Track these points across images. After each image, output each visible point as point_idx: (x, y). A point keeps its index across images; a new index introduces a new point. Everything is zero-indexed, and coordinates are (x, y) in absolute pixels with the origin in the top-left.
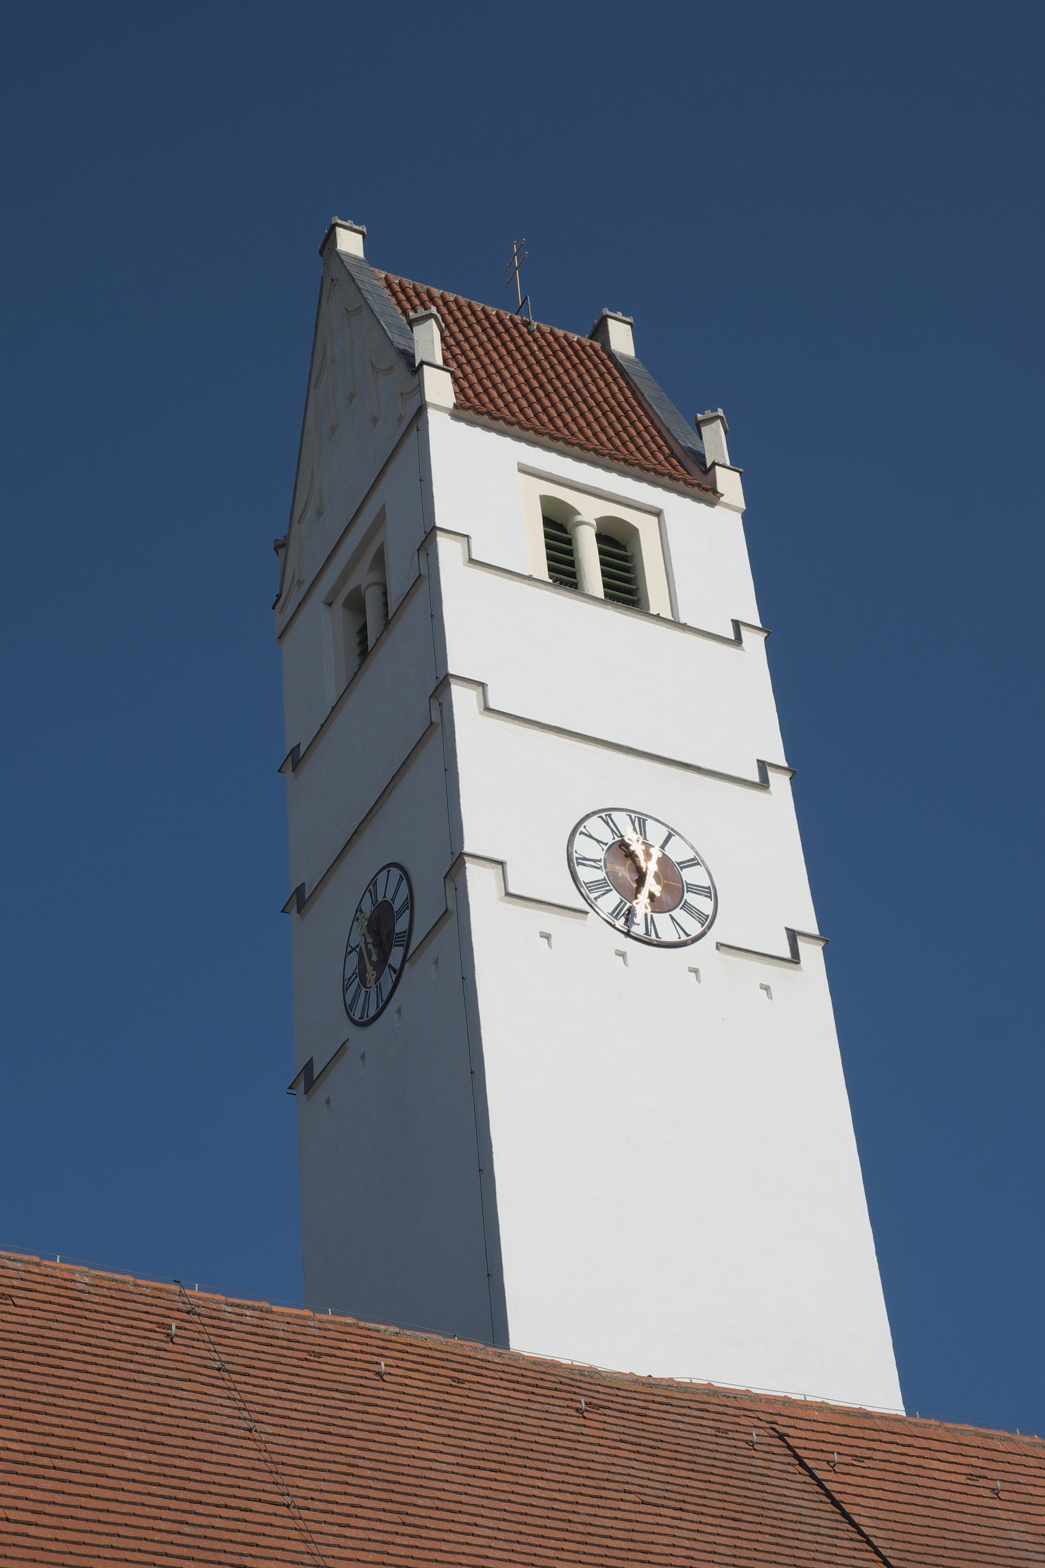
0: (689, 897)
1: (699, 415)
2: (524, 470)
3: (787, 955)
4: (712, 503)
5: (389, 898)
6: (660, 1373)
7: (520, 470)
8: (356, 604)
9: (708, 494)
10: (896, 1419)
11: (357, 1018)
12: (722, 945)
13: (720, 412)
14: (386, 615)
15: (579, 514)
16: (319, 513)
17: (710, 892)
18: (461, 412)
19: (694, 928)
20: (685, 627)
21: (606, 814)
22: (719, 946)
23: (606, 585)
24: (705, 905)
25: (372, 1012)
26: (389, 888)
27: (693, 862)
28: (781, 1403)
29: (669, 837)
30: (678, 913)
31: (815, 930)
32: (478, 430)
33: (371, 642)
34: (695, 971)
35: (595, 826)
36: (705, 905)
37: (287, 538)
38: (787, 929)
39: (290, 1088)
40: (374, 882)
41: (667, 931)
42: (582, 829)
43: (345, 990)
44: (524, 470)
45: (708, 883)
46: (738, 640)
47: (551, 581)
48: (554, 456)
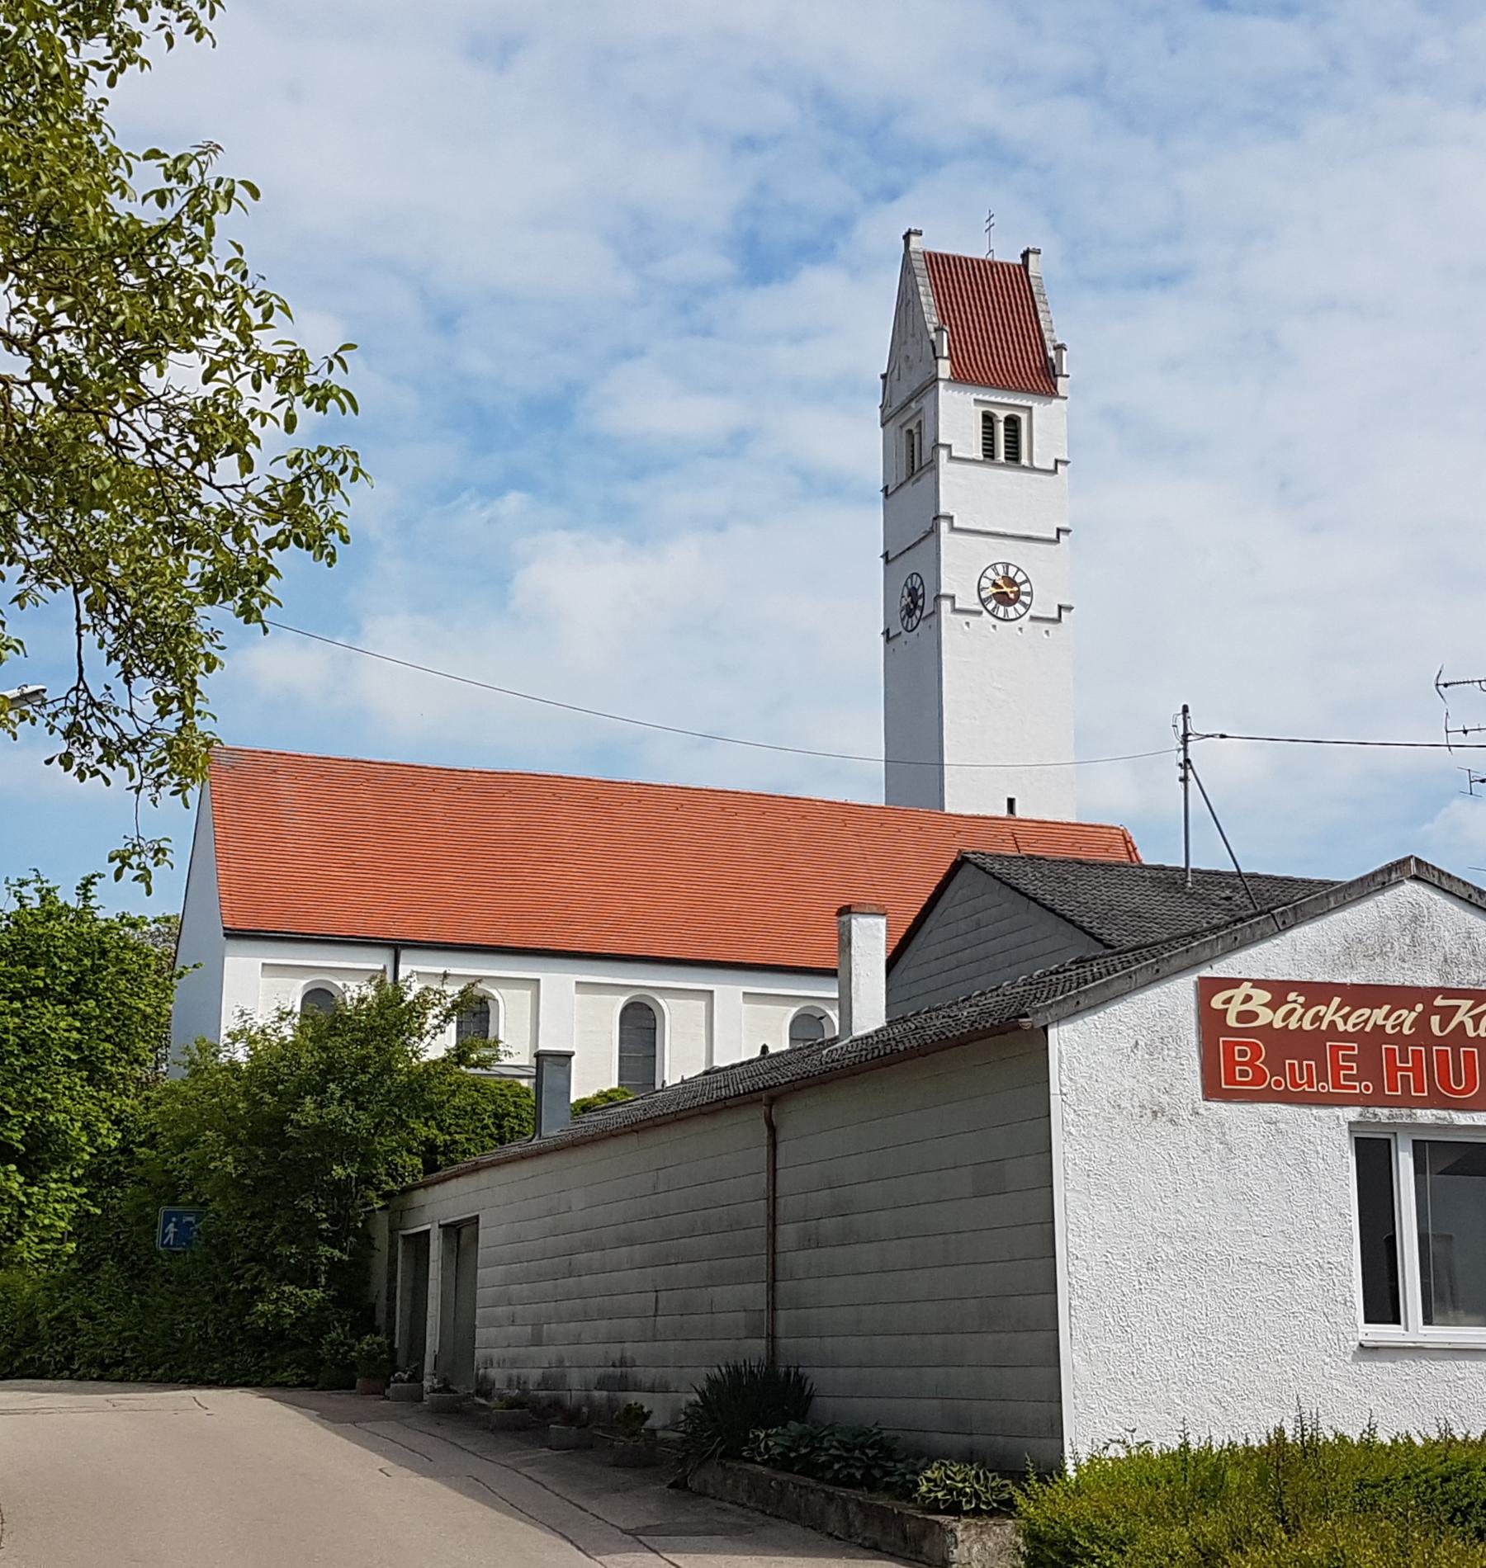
30: (1017, 606)
41: (1012, 614)
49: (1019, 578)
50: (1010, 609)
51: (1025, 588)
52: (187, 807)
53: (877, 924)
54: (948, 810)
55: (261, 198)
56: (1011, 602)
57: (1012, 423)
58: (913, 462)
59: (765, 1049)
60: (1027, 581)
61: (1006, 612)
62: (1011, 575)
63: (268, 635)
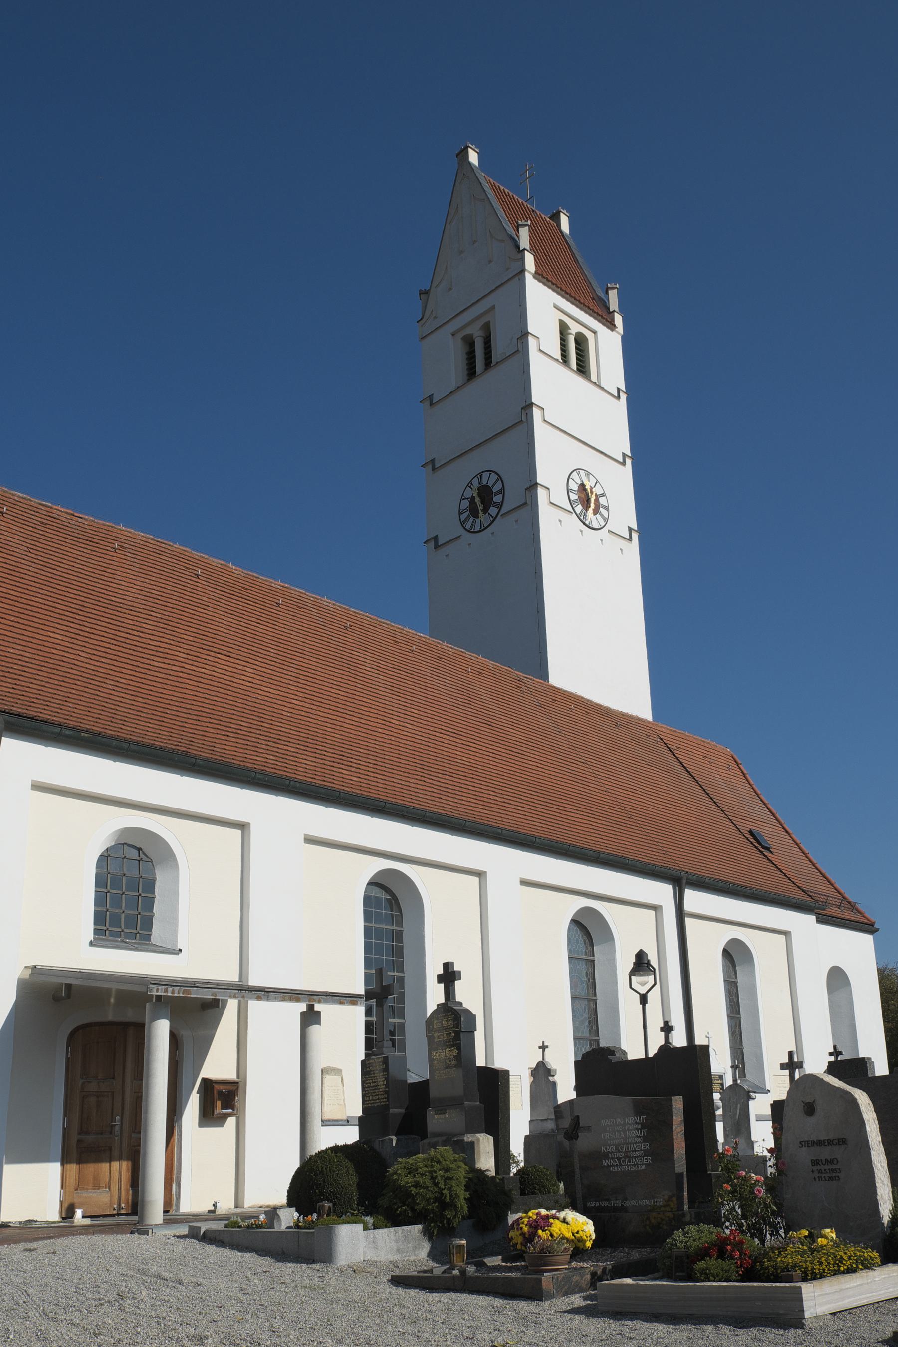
1: (609, 285)
2: (556, 307)
3: (628, 537)
4: (612, 330)
5: (490, 484)
6: (625, 710)
7: (555, 307)
9: (611, 326)
10: (649, 722)
13: (618, 286)
15: (570, 329)
17: (606, 508)
18: (537, 276)
20: (602, 389)
22: (609, 531)
23: (577, 364)
31: (636, 528)
32: (541, 284)
34: (601, 540)
37: (429, 290)
38: (629, 527)
39: (424, 543)
42: (492, 519)
44: (556, 307)
45: (607, 505)
47: (562, 361)
48: (564, 300)
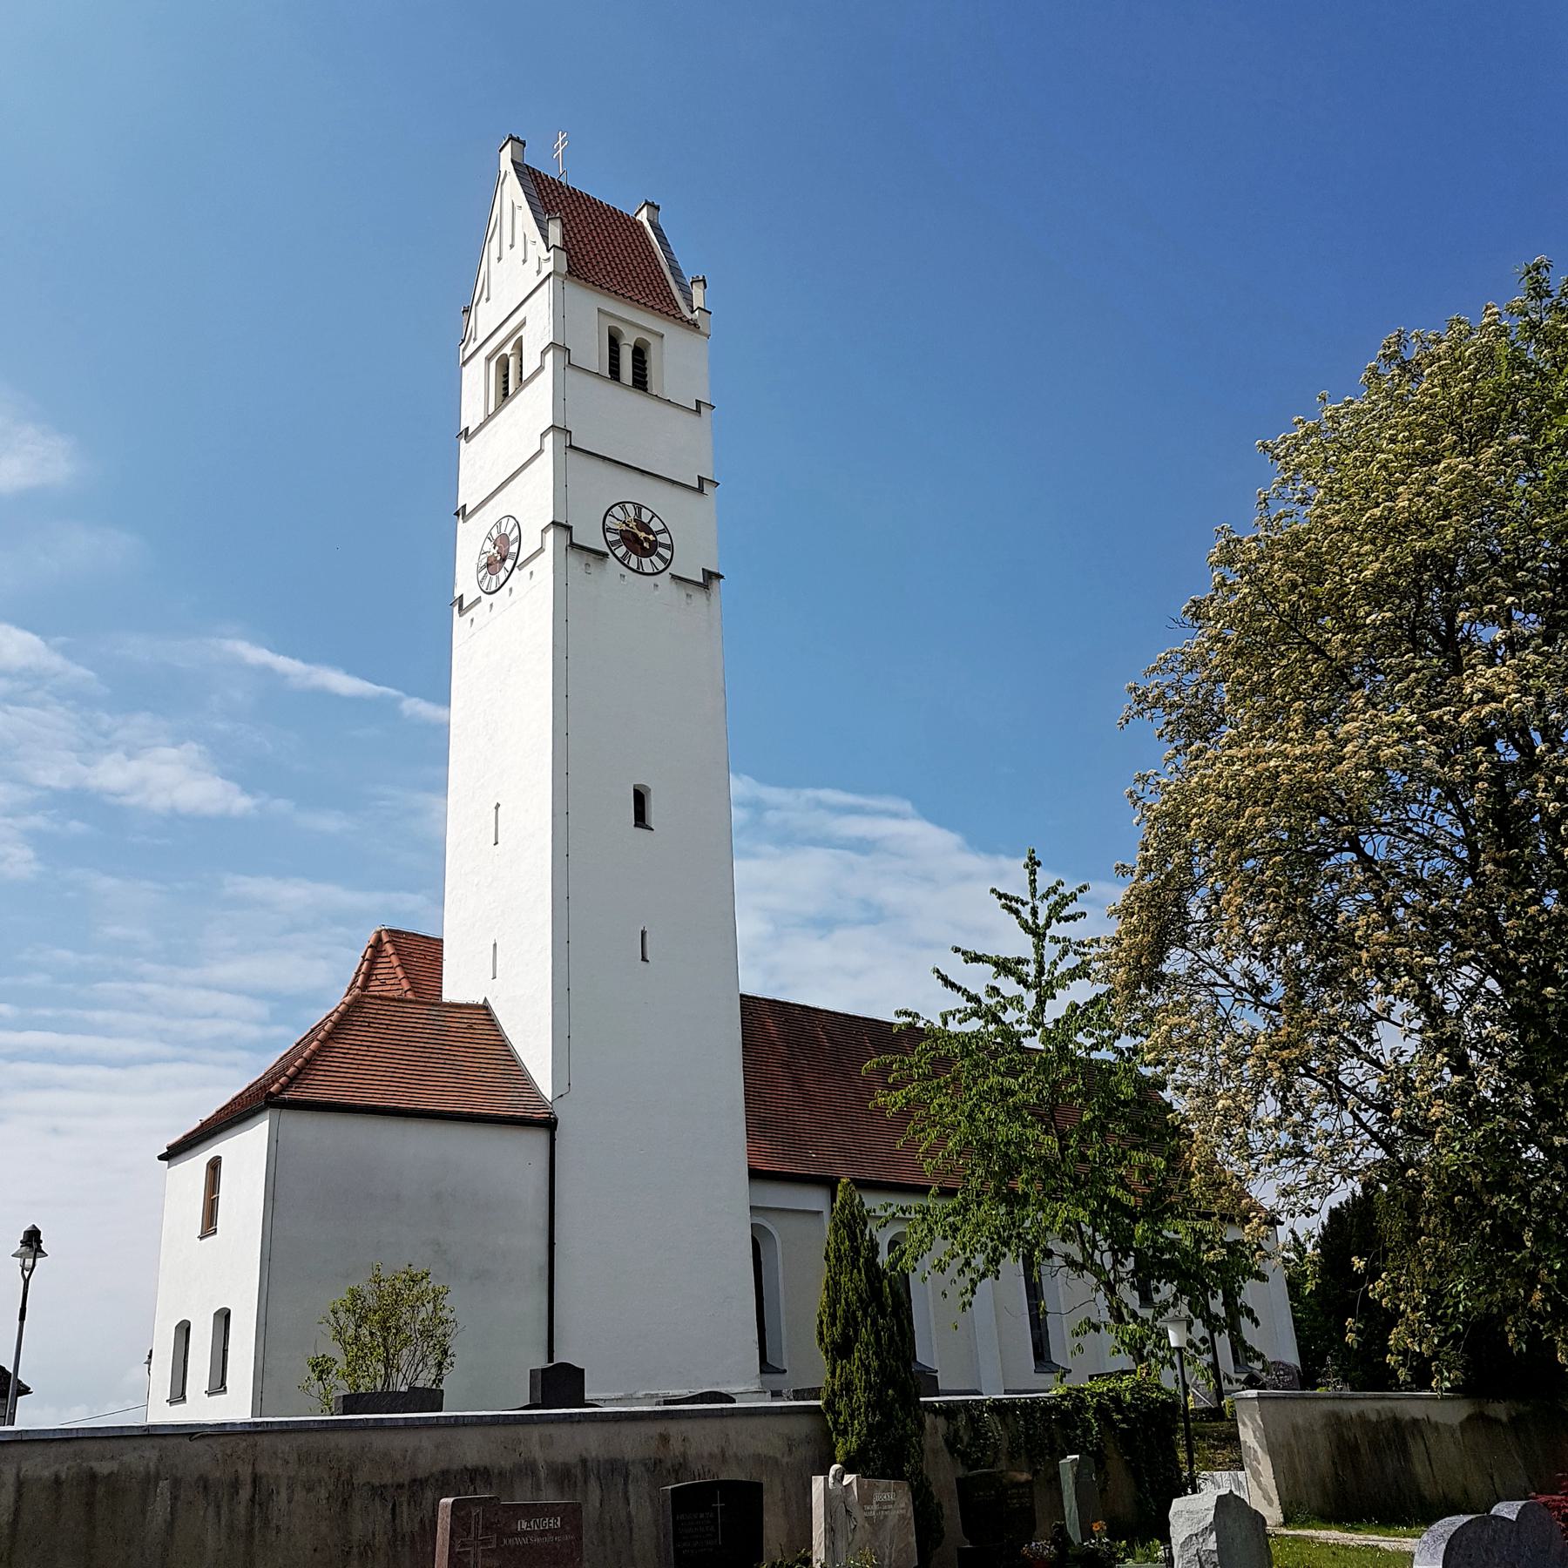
0: (659, 549)
5: (507, 533)
8: (504, 364)
11: (484, 588)
12: (188, 1330)
14: (521, 379)
16: (488, 300)
17: (670, 547)
19: (661, 566)
21: (622, 504)
22: (673, 576)
24: (667, 554)
25: (493, 589)
26: (508, 526)
27: (665, 530)
28: (1546, 1548)
29: (653, 517)
30: (654, 558)
33: (511, 391)
35: (617, 511)
36: (667, 554)
40: (500, 521)
41: (648, 568)
43: (478, 572)
46: (698, 411)
49: (655, 525)
50: (645, 561)
51: (662, 538)
52: (896, 1013)
53: (1513, 1512)
54: (447, 997)
55: (27, 1227)
56: (647, 553)
57: (639, 353)
58: (506, 382)
59: (25, 1390)
60: (665, 530)
61: (640, 563)
62: (645, 519)
63: (941, 1290)
